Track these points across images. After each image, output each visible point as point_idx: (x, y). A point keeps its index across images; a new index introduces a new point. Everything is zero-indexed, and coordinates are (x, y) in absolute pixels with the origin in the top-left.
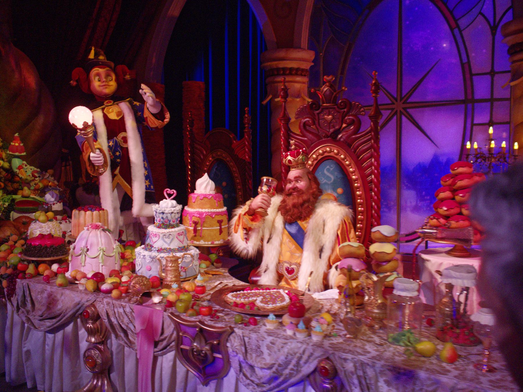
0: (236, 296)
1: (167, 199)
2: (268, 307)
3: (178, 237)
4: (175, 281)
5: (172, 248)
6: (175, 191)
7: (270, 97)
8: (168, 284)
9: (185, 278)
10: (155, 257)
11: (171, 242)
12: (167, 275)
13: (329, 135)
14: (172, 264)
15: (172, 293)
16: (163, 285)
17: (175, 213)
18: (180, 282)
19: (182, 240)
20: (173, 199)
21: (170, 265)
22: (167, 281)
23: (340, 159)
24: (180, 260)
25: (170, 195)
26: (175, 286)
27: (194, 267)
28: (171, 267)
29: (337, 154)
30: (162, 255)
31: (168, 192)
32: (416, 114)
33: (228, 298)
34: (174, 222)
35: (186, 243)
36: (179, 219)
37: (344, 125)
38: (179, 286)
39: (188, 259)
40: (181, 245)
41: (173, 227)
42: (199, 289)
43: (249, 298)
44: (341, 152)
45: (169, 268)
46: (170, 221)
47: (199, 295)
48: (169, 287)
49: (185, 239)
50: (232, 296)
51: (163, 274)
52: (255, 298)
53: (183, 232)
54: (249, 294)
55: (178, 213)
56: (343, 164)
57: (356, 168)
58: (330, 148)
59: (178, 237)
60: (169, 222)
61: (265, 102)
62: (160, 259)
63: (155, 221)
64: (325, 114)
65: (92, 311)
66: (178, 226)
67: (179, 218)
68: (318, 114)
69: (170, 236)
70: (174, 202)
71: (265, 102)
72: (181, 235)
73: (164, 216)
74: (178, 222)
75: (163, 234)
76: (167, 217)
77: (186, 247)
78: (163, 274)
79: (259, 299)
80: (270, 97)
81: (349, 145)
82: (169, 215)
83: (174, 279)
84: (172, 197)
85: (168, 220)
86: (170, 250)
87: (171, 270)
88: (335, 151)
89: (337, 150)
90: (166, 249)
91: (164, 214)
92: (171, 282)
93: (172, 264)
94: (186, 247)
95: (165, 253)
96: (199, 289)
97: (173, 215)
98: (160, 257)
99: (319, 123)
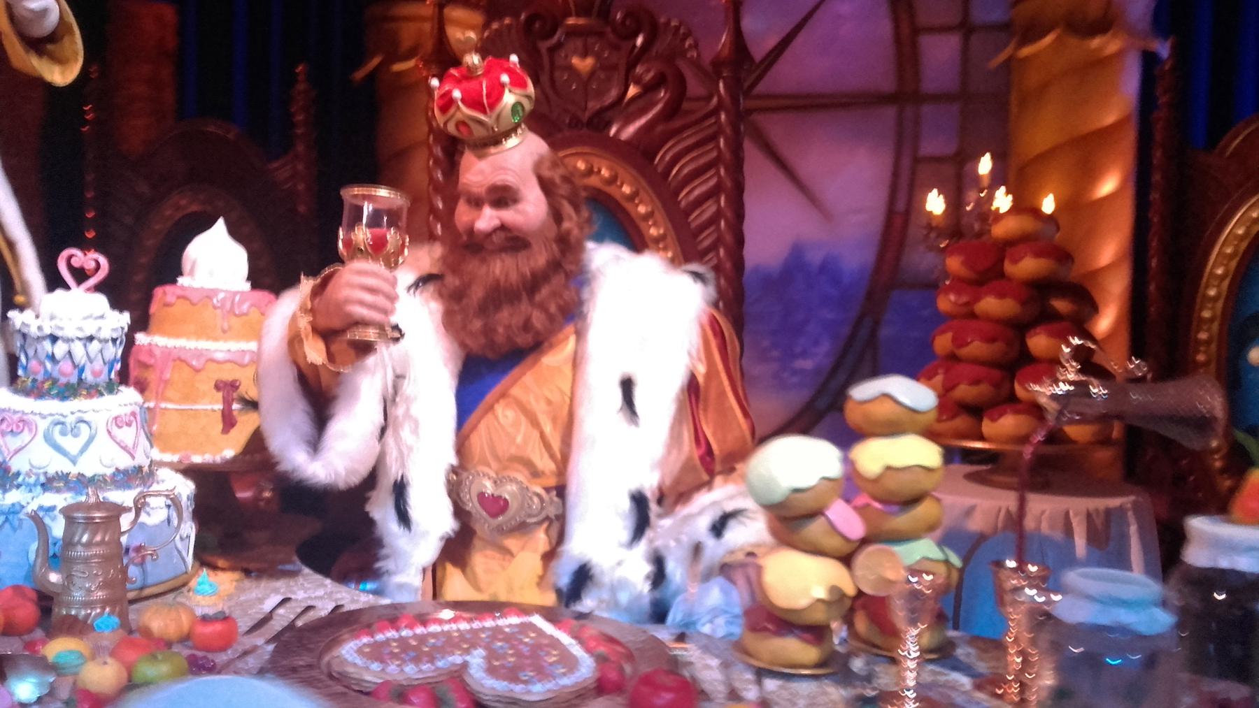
0: (377, 653)
1: (67, 287)
2: (529, 692)
3: (115, 430)
4: (104, 603)
5: (89, 474)
6: (103, 261)
7: (376, 61)
8: (75, 618)
9: (142, 589)
10: (18, 508)
11: (83, 451)
12: (69, 577)
13: (585, 120)
14: (94, 534)
15: (96, 653)
16: (54, 618)
17: (106, 341)
18: (126, 603)
19: (130, 443)
20: (98, 288)
21: (85, 538)
22: (69, 605)
23: (618, 197)
24: (125, 521)
25: (80, 275)
26: (107, 622)
27: (179, 545)
28: (89, 545)
29: (612, 180)
30: (49, 499)
31: (76, 263)
32: (760, 119)
33: (344, 662)
34: (96, 374)
35: (145, 454)
36: (118, 366)
37: (632, 91)
38: (125, 625)
39: (156, 514)
40: (125, 462)
41: (94, 391)
42: (209, 629)
43: (432, 660)
44: (622, 173)
45: (80, 551)
46: (82, 370)
47: (210, 656)
48: (75, 627)
49: (144, 441)
50: (360, 651)
51: (54, 577)
52: (457, 659)
53: (133, 414)
54: (422, 639)
55: (114, 340)
56: (628, 214)
57: (670, 226)
58: (587, 162)
59: (115, 430)
60: (76, 372)
61: (360, 74)
62: (41, 514)
63: (20, 372)
64: (575, 52)
65: (528, 636)
66: (111, 388)
67: (115, 360)
68: (553, 50)
69: (83, 427)
70: (101, 301)
71: (360, 74)
72: (129, 424)
73: (60, 349)
74: (113, 375)
75: (50, 419)
76: (70, 353)
77: (146, 469)
78: (54, 577)
79: (476, 659)
80: (376, 61)
81: (649, 155)
82: (78, 350)
83: (100, 594)
84: (92, 282)
85: (75, 366)
86: (82, 482)
87: (86, 560)
88: (605, 173)
89: (610, 168)
90: (64, 477)
91: (59, 343)
92: (88, 604)
93: (94, 534)
94: (146, 469)
95: (58, 491)
96: (209, 629)
97: (94, 347)
98: (41, 508)
99: (552, 81)
